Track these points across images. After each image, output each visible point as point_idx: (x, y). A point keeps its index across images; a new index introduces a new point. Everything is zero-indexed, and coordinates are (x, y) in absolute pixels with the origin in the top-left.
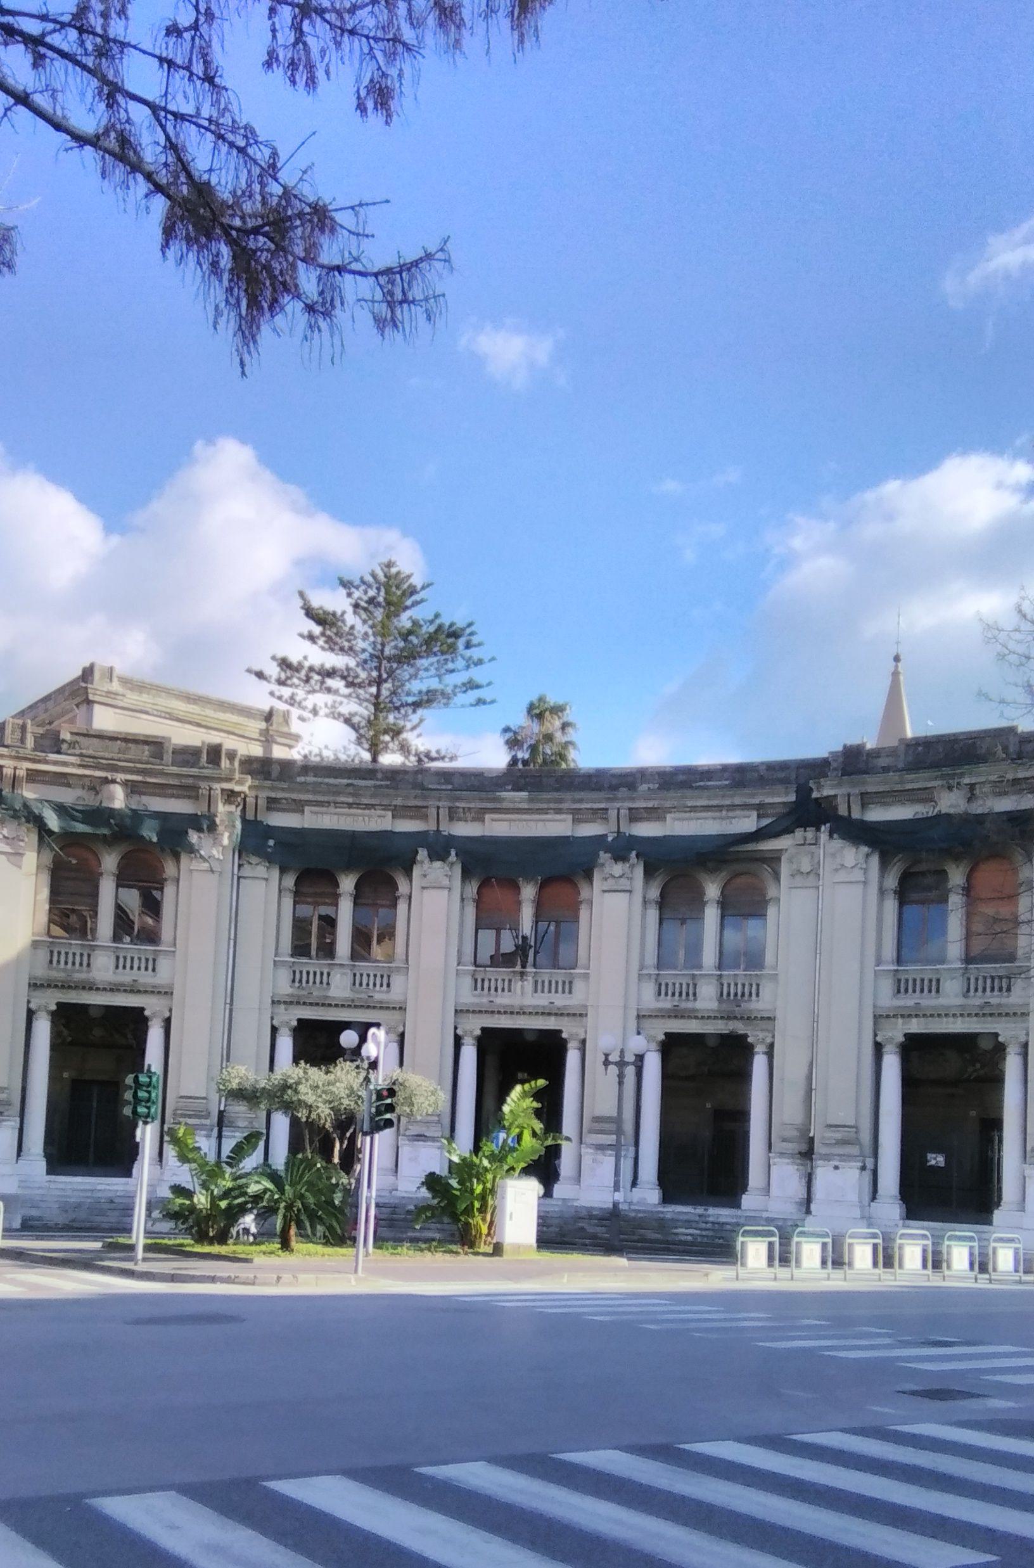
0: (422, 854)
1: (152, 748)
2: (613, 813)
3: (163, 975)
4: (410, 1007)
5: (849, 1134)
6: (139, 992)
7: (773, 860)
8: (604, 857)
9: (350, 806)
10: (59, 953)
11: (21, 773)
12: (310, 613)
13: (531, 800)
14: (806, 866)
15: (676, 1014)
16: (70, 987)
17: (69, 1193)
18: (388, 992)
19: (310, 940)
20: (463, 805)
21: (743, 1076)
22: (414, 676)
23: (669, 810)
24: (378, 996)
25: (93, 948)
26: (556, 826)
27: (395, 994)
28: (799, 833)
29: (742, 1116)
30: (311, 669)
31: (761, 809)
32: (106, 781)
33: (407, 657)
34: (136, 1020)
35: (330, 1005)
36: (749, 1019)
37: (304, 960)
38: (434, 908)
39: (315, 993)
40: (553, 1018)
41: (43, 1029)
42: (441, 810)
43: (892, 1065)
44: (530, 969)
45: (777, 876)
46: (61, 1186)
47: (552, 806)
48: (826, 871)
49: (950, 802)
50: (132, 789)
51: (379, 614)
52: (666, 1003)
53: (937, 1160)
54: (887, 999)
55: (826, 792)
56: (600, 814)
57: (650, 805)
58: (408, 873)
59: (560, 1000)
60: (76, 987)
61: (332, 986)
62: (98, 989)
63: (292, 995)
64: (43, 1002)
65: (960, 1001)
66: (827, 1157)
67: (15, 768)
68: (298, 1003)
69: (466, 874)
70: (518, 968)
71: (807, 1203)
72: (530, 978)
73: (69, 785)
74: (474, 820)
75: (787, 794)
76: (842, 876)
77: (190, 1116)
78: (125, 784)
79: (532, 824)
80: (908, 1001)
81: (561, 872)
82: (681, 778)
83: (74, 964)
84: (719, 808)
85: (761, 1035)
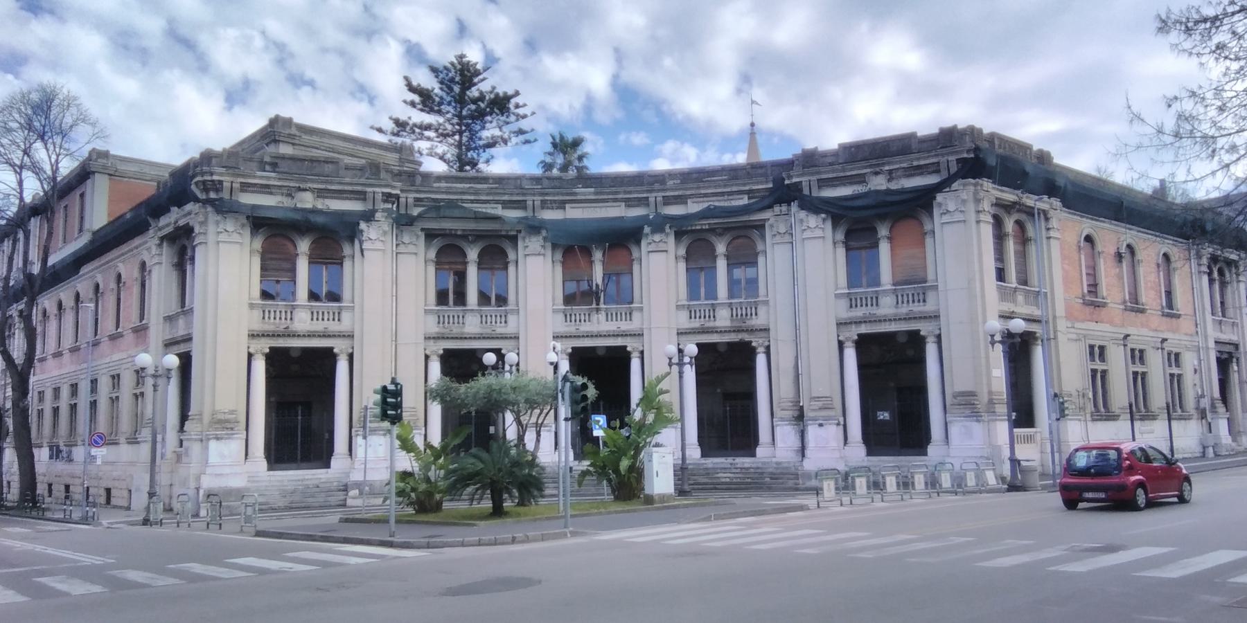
3: (345, 324)
7: (760, 227)
12: (412, 89)
13: (596, 193)
14: (782, 230)
19: (450, 296)
21: (751, 370)
22: (483, 128)
25: (294, 307)
28: (777, 209)
29: (751, 396)
30: (415, 125)
31: (750, 193)
33: (480, 116)
34: (326, 358)
36: (751, 331)
37: (445, 308)
41: (260, 367)
43: (851, 355)
44: (602, 306)
45: (763, 237)
48: (797, 231)
49: (879, 183)
51: (457, 89)
52: (696, 324)
53: (884, 416)
54: (845, 313)
55: (795, 180)
56: (644, 202)
64: (761, 341)
66: (815, 419)
70: (594, 306)
71: (802, 450)
73: (271, 193)
75: (767, 182)
76: (778, 239)
80: (859, 313)
81: (621, 240)
85: (761, 341)
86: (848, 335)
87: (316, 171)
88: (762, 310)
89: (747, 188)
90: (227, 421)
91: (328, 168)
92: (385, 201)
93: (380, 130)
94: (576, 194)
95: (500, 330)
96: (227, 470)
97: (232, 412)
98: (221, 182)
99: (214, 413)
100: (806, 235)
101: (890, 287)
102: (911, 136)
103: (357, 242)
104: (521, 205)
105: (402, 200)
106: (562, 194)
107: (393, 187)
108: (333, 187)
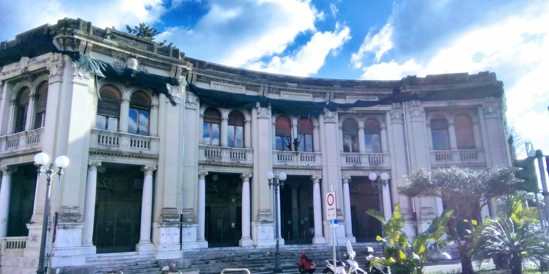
0: (258, 104)
1: (148, 46)
2: (328, 94)
4: (255, 166)
6: (142, 157)
7: (383, 114)
9: (229, 82)
10: (103, 137)
11: (90, 45)
13: (298, 87)
14: (397, 116)
15: (355, 169)
16: (109, 154)
17: (112, 262)
18: (246, 160)
20: (273, 86)
23: (348, 94)
24: (242, 162)
27: (249, 161)
28: (394, 105)
32: (131, 56)
34: (138, 173)
35: (222, 166)
38: (261, 126)
39: (216, 160)
40: (308, 171)
42: (266, 88)
45: (384, 120)
46: (106, 259)
48: (408, 117)
50: (142, 62)
52: (351, 165)
55: (408, 90)
56: (323, 95)
57: (341, 92)
59: (311, 164)
60: (113, 154)
62: (123, 156)
63: (206, 161)
65: (460, 162)
67: (87, 42)
68: (209, 165)
69: (273, 113)
72: (299, 155)
73: (111, 56)
74: (276, 93)
75: (389, 91)
77: (170, 218)
78: (139, 59)
79: (298, 96)
81: (308, 113)
82: (348, 84)
83: (110, 143)
89: (379, 93)
90: (73, 215)
96: (69, 253)
97: (76, 208)
98: (79, 41)
100: (414, 119)
102: (466, 74)
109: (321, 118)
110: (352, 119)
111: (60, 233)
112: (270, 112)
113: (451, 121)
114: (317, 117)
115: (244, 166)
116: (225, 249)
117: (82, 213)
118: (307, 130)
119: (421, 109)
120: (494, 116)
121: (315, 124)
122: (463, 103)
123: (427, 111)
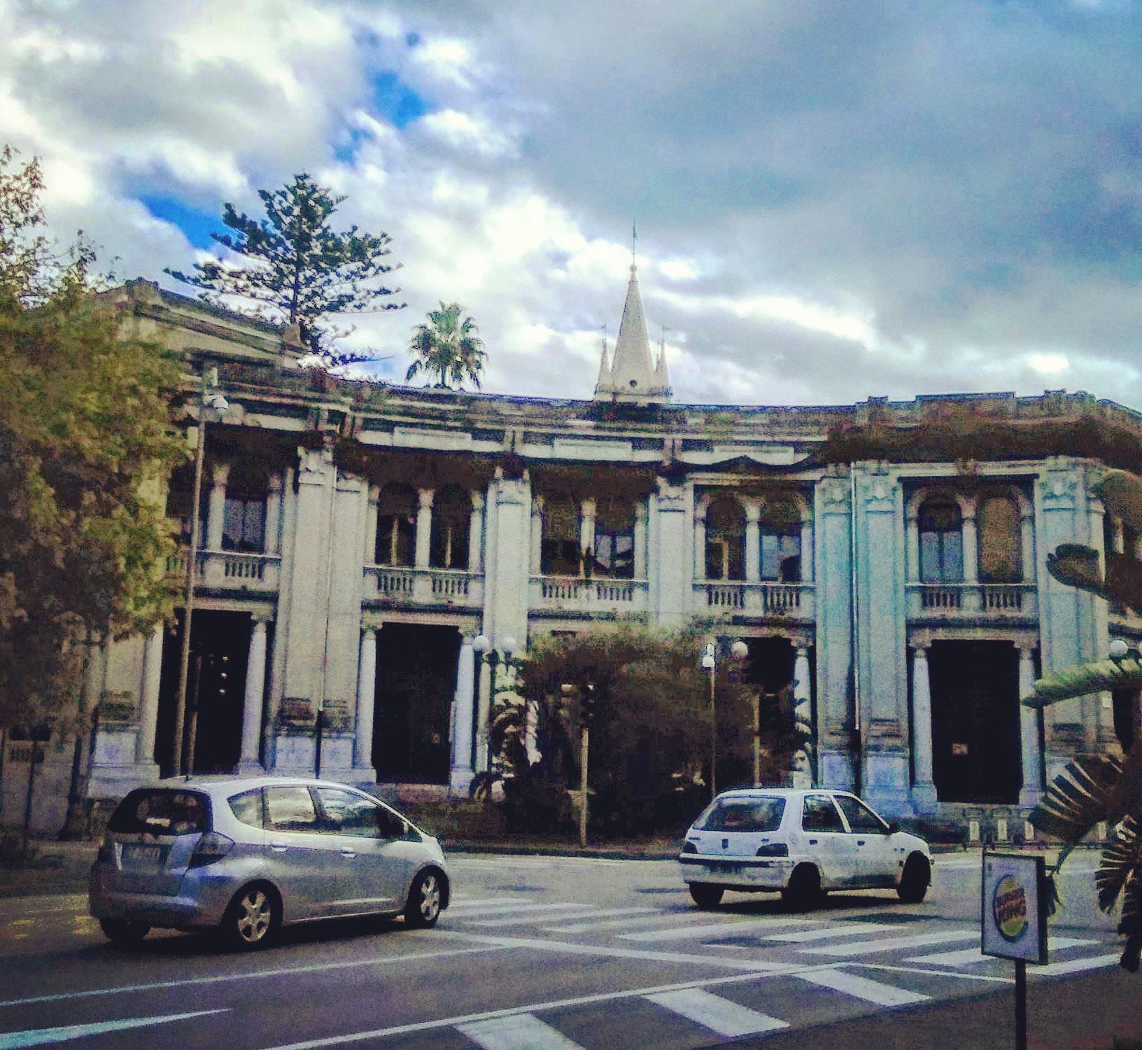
0: (499, 472)
3: (269, 581)
4: (486, 611)
5: (893, 729)
7: (807, 490)
8: (661, 481)
13: (597, 428)
26: (619, 452)
36: (793, 625)
47: (615, 434)
53: (960, 749)
54: (917, 611)
56: (658, 444)
58: (484, 491)
61: (415, 593)
64: (803, 640)
79: (596, 450)
81: (623, 492)
84: (762, 443)
86: (920, 641)
87: (248, 376)
88: (805, 598)
89: (794, 439)
90: (121, 706)
91: (262, 372)
92: (330, 421)
93: (178, 275)
94: (567, 427)
95: (458, 600)
96: (117, 774)
97: (126, 694)
99: (104, 694)
101: (976, 584)
103: (290, 472)
104: (497, 436)
105: (349, 420)
106: (552, 426)
107: (342, 403)
108: (272, 400)
109: (652, 499)
110: (733, 501)
111: (102, 738)
112: (527, 489)
113: (968, 511)
114: (645, 499)
115: (462, 611)
116: (406, 787)
117: (136, 704)
118: (618, 524)
119: (892, 480)
120: (1066, 503)
121: (640, 512)
122: (992, 469)
123: (909, 485)
